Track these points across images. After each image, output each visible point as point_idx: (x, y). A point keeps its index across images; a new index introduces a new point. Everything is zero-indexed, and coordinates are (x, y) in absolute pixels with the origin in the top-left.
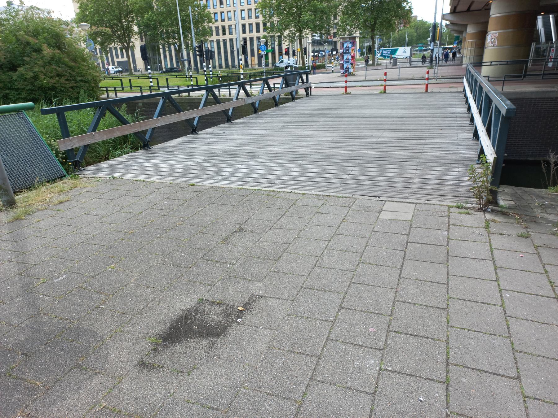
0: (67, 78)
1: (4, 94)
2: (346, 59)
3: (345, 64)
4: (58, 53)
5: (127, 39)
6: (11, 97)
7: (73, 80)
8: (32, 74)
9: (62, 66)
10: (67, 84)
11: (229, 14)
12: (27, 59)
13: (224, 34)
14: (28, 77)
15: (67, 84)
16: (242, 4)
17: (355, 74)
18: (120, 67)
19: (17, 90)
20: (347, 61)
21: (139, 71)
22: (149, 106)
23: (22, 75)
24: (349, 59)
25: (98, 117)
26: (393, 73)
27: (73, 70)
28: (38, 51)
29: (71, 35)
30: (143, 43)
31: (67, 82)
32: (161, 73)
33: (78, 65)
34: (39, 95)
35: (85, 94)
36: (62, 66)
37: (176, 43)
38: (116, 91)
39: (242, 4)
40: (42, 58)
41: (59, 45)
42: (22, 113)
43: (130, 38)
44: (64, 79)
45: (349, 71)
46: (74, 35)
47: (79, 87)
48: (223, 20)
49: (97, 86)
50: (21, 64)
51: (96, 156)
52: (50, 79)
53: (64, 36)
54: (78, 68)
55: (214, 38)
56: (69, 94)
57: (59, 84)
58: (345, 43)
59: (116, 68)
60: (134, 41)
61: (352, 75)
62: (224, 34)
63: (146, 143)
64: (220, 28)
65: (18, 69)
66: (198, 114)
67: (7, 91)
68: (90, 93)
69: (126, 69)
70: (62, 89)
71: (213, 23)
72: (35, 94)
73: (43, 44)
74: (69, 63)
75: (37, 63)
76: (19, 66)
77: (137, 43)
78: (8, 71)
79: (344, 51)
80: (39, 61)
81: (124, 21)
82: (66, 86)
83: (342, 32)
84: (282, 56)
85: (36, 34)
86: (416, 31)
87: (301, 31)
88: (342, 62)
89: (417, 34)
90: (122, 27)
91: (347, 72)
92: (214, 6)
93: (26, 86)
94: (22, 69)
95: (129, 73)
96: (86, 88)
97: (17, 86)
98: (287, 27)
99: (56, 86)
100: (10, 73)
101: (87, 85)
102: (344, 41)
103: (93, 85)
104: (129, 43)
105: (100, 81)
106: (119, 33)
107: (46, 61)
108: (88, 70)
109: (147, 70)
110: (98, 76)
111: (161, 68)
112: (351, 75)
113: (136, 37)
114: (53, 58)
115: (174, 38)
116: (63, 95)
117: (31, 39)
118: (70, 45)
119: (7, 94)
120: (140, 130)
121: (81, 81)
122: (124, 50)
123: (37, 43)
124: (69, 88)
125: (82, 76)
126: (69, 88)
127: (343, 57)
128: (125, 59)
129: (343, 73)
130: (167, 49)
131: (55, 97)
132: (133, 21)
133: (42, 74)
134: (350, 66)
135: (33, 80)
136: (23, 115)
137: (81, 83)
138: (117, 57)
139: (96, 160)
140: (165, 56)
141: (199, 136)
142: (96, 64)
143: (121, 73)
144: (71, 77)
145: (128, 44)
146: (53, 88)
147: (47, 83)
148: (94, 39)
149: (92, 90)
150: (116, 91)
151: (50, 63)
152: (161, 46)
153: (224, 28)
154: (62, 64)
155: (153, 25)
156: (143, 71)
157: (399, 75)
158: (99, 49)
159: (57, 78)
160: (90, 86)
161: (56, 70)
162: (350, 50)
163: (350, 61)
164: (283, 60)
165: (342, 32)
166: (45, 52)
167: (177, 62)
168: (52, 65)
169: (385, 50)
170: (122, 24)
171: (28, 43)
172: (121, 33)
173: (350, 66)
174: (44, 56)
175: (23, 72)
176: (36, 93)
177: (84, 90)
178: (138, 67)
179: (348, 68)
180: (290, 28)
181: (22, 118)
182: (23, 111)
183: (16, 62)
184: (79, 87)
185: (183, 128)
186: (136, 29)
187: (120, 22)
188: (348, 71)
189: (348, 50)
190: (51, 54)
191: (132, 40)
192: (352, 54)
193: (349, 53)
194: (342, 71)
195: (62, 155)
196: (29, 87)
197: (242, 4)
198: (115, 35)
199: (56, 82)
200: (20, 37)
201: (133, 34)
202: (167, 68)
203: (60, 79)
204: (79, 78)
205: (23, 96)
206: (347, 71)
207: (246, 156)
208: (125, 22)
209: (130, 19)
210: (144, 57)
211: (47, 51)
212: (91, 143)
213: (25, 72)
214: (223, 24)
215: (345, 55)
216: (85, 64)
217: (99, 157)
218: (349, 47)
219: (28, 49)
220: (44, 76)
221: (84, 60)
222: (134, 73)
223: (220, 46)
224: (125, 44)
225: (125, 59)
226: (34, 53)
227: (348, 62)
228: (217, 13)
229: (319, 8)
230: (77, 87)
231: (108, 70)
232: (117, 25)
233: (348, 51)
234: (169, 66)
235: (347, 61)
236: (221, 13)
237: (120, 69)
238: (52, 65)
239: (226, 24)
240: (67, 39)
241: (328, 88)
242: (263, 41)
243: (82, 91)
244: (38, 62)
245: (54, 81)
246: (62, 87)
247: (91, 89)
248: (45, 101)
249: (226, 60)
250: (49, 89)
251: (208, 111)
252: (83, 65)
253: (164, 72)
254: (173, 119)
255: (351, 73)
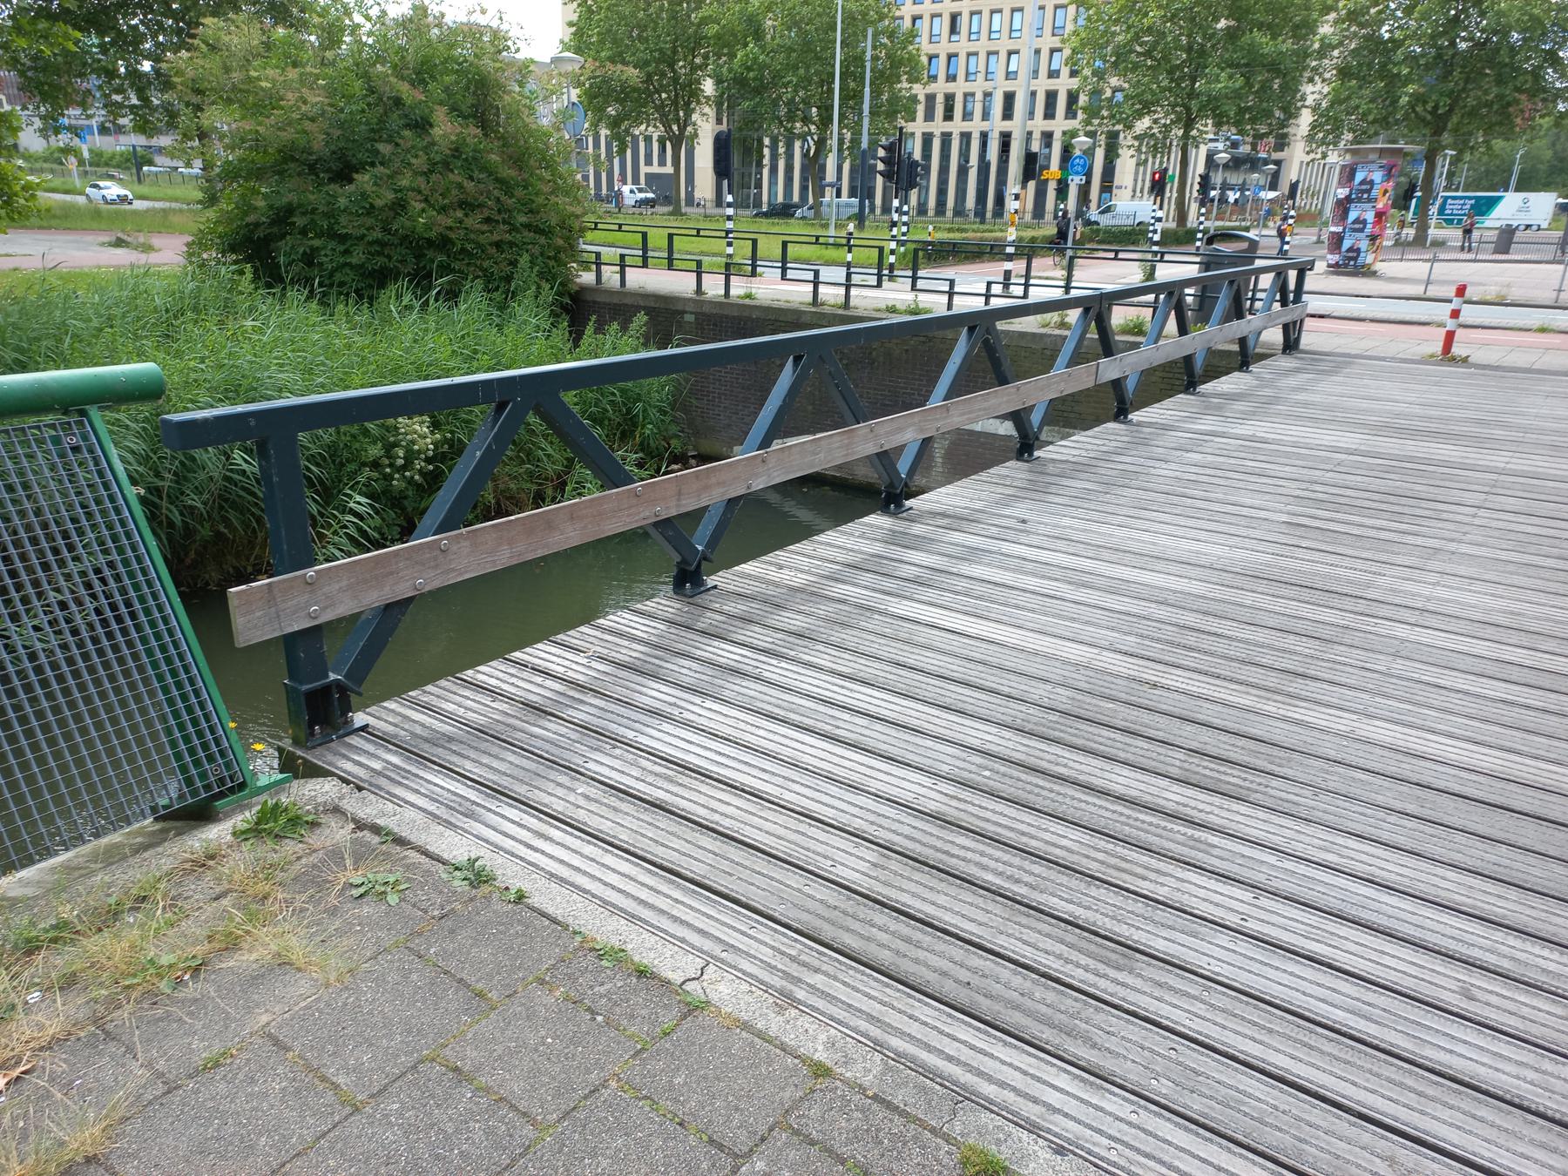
0: (486, 213)
1: (308, 251)
2: (1357, 221)
3: (1347, 234)
4: (475, 137)
5: (681, 114)
6: (325, 259)
7: (504, 222)
8: (390, 196)
9: (481, 176)
10: (483, 233)
11: (973, 60)
12: (385, 149)
13: (948, 116)
14: (379, 203)
15: (483, 233)
16: (1014, 35)
17: (1375, 272)
18: (651, 188)
19: (343, 238)
20: (1357, 226)
21: (698, 205)
22: (715, 325)
23: (364, 196)
24: (1364, 222)
25: (482, 456)
26: (1486, 275)
27: (509, 192)
28: (422, 125)
29: (521, 84)
30: (724, 127)
31: (485, 227)
32: (756, 215)
33: (526, 176)
34: (401, 262)
35: (531, 268)
36: (481, 176)
37: (811, 134)
38: (623, 266)
39: (1014, 34)
40: (426, 149)
41: (483, 114)
42: (81, 422)
43: (688, 114)
44: (479, 217)
45: (1360, 261)
46: (531, 85)
47: (517, 246)
48: (951, 78)
49: (572, 247)
50: (367, 163)
51: (531, 474)
52: (439, 213)
53: (501, 87)
54: (525, 187)
55: (918, 127)
56: (486, 264)
57: (462, 232)
58: (1360, 166)
59: (640, 190)
60: (699, 122)
61: (1367, 272)
62: (948, 116)
63: (693, 568)
64: (940, 99)
65: (355, 176)
66: (922, 430)
67: (317, 243)
68: (546, 265)
69: (666, 197)
70: (468, 247)
71: (925, 84)
72: (389, 257)
73: (436, 107)
74: (500, 170)
75: (409, 164)
76: (360, 167)
77: (706, 127)
78: (331, 180)
79: (1351, 194)
80: (416, 156)
81: (681, 63)
82: (482, 239)
83: (1328, 132)
84: (1111, 192)
85: (423, 73)
86: (1554, 144)
87: (1189, 124)
88: (1340, 229)
89: (1555, 153)
90: (675, 80)
91: (1352, 263)
92: (931, 36)
93: (368, 229)
94: (367, 177)
95: (671, 208)
96: (536, 250)
97: (344, 227)
98: (1146, 108)
99: (453, 236)
100: (333, 188)
101: (543, 240)
102: (1356, 159)
103: (560, 242)
104: (685, 126)
105: (583, 230)
106: (664, 95)
107: (438, 158)
108: (552, 193)
109: (719, 202)
110: (577, 217)
111: (758, 204)
112: (1364, 275)
113: (707, 110)
114: (457, 151)
115: (806, 120)
116: (469, 264)
117: (405, 90)
118: (514, 115)
119: (315, 250)
120: (673, 512)
121: (528, 226)
122: (668, 144)
123: (421, 102)
124: (490, 245)
125: (531, 211)
126: (490, 245)
127: (1346, 212)
128: (669, 169)
129: (1337, 265)
130: (781, 150)
131: (445, 269)
132: (707, 65)
133: (419, 197)
134: (1364, 245)
135: (392, 214)
136: (85, 438)
137: (526, 233)
138: (649, 162)
139: (529, 485)
140: (774, 170)
141: (917, 529)
142: (579, 177)
143: (653, 207)
144: (499, 211)
145: (682, 129)
146: (443, 243)
147: (428, 227)
148: (600, 110)
149: (555, 258)
150: (623, 266)
151: (446, 165)
152: (767, 141)
153: (949, 98)
154: (483, 169)
155: (755, 79)
156: (709, 205)
157: (1560, 291)
158: (606, 137)
159: (459, 214)
160: (549, 245)
161: (460, 186)
162: (1374, 193)
163: (1369, 226)
164: (1109, 207)
165: (1328, 132)
166: (437, 132)
167: (804, 189)
168: (452, 171)
169: (1454, 198)
170: (674, 71)
171: (398, 102)
172: (669, 97)
173: (1364, 245)
174: (433, 144)
175: (369, 188)
176: (392, 254)
177: (531, 255)
178: (698, 195)
179: (1358, 251)
180: (1155, 112)
181: (76, 449)
182: (94, 413)
183: (354, 155)
184: (517, 246)
185: (810, 408)
186: (708, 87)
187: (672, 66)
188: (1355, 259)
189: (1369, 191)
190: (453, 138)
191: (695, 117)
192: (1380, 205)
193: (1369, 200)
194: (1333, 258)
195: (423, 464)
196: (377, 234)
197: (1014, 34)
198: (653, 102)
199: (453, 225)
200: (377, 83)
201: (698, 102)
202: (773, 202)
203: (466, 215)
204: (522, 219)
205: (354, 261)
206: (1350, 259)
207: (1233, 777)
208: (684, 66)
209: (698, 60)
210: (722, 168)
211: (445, 128)
212: (427, 588)
213: (374, 188)
214: (951, 87)
215: (1353, 205)
216: (546, 175)
217: (539, 477)
218: (1372, 183)
219: (395, 121)
220: (423, 205)
221: (550, 165)
222: (683, 210)
223: (931, 151)
224: (675, 128)
225: (669, 169)
226: (407, 133)
227: (1362, 230)
228: (937, 56)
229: (1262, 55)
230: (512, 244)
231: (619, 194)
232: (663, 75)
233: (1365, 196)
234: (780, 199)
235: (1357, 226)
236: (950, 57)
237: (651, 195)
238: (452, 171)
239: (959, 88)
240: (506, 97)
241: (1322, 316)
242: (1086, 142)
243: (524, 260)
244: (414, 161)
245: (450, 222)
246: (469, 241)
247: (552, 254)
248: (410, 282)
249: (942, 192)
250: (430, 242)
251: (964, 414)
252: (541, 179)
253: (766, 215)
254: (822, 455)
255: (1363, 267)
